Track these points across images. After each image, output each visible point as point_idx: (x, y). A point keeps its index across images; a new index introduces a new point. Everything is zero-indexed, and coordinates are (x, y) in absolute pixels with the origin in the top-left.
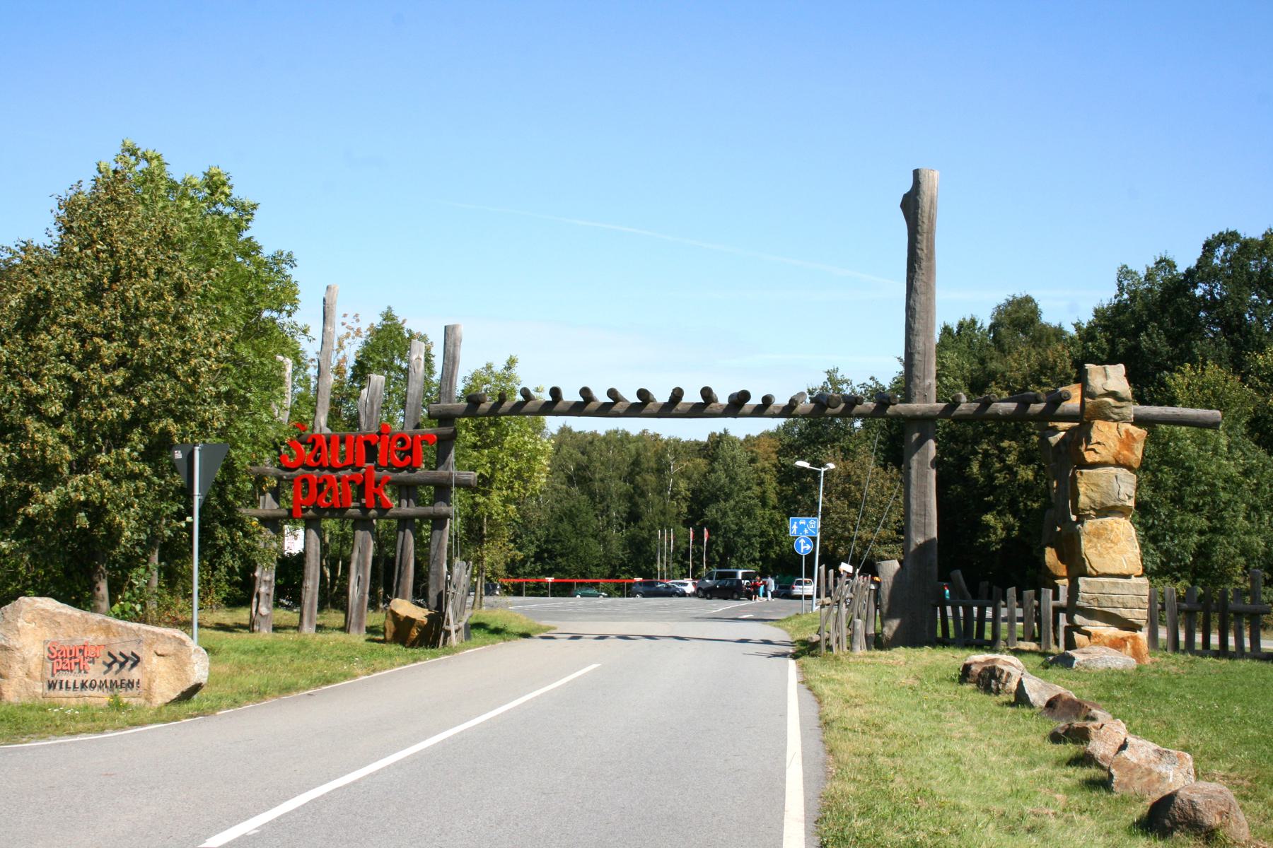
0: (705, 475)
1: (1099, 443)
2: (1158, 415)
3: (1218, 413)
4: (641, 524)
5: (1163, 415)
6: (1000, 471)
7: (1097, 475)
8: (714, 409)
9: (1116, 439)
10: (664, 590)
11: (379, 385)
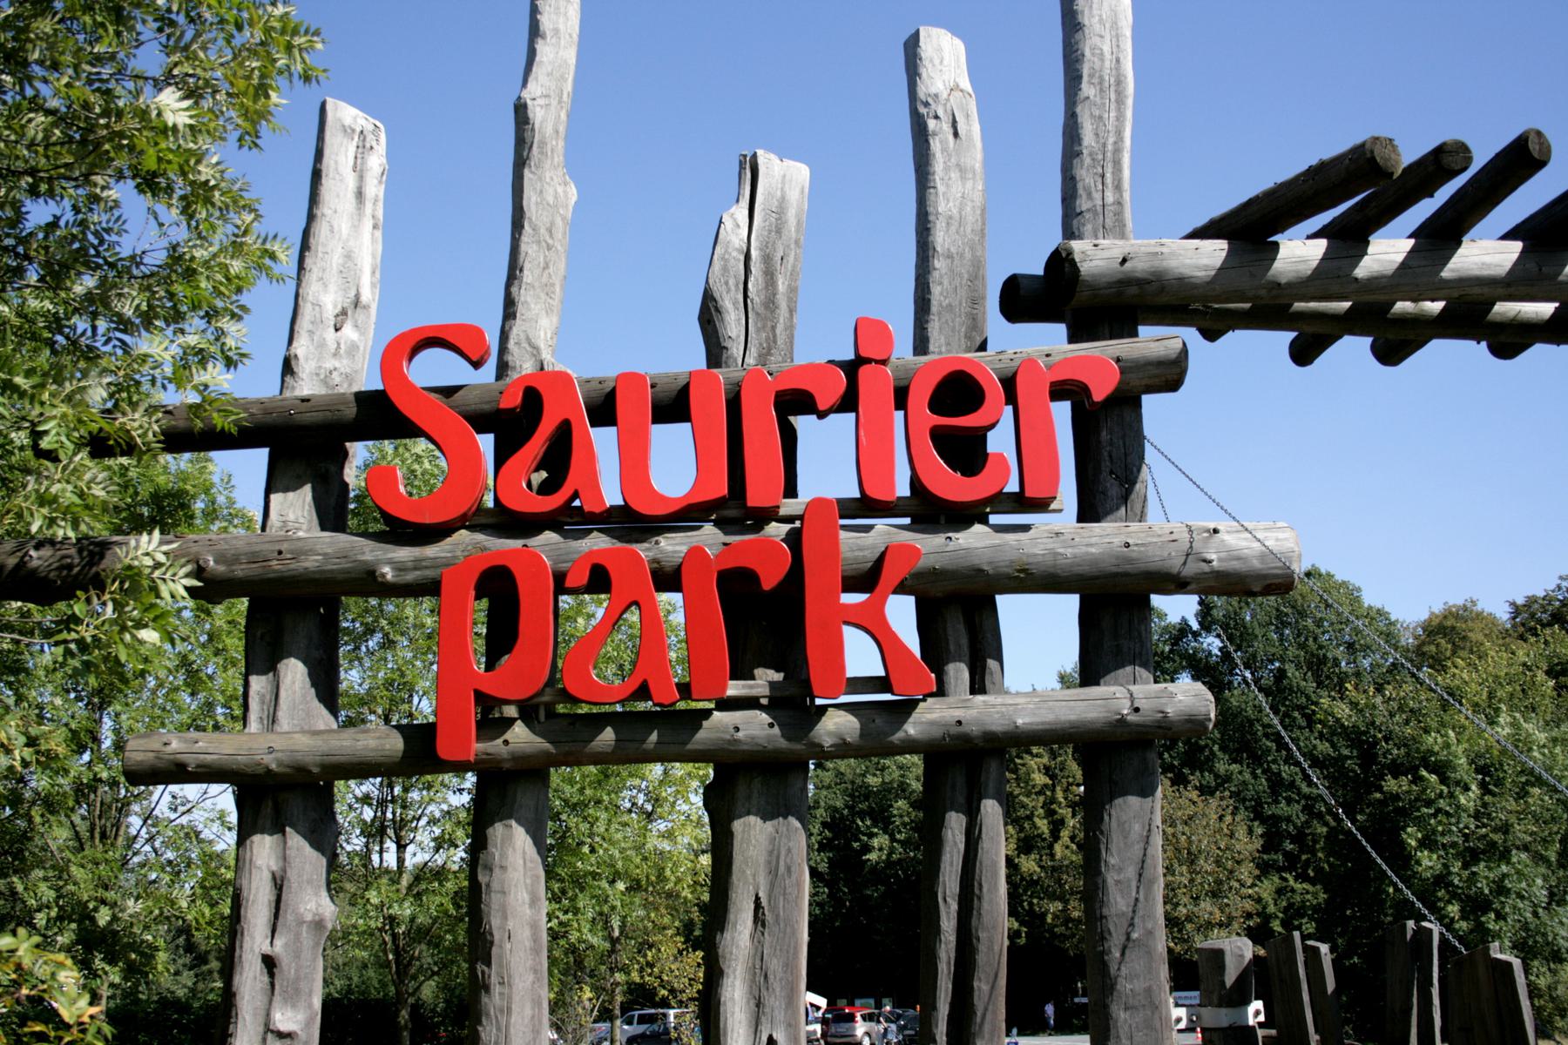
11: (794, 196)
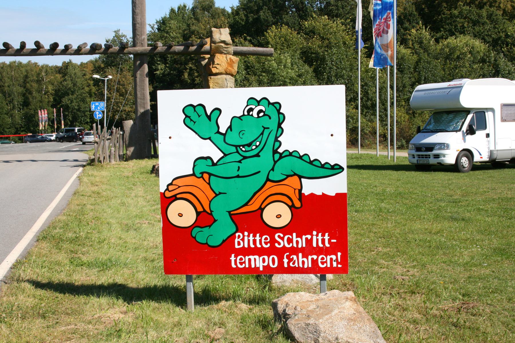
0: (61, 82)
1: (218, 64)
2: (246, 51)
3: (272, 49)
4: (30, 107)
5: (249, 51)
6: (197, 77)
7: (218, 78)
8: (42, 52)
9: (226, 63)
10: (40, 139)
